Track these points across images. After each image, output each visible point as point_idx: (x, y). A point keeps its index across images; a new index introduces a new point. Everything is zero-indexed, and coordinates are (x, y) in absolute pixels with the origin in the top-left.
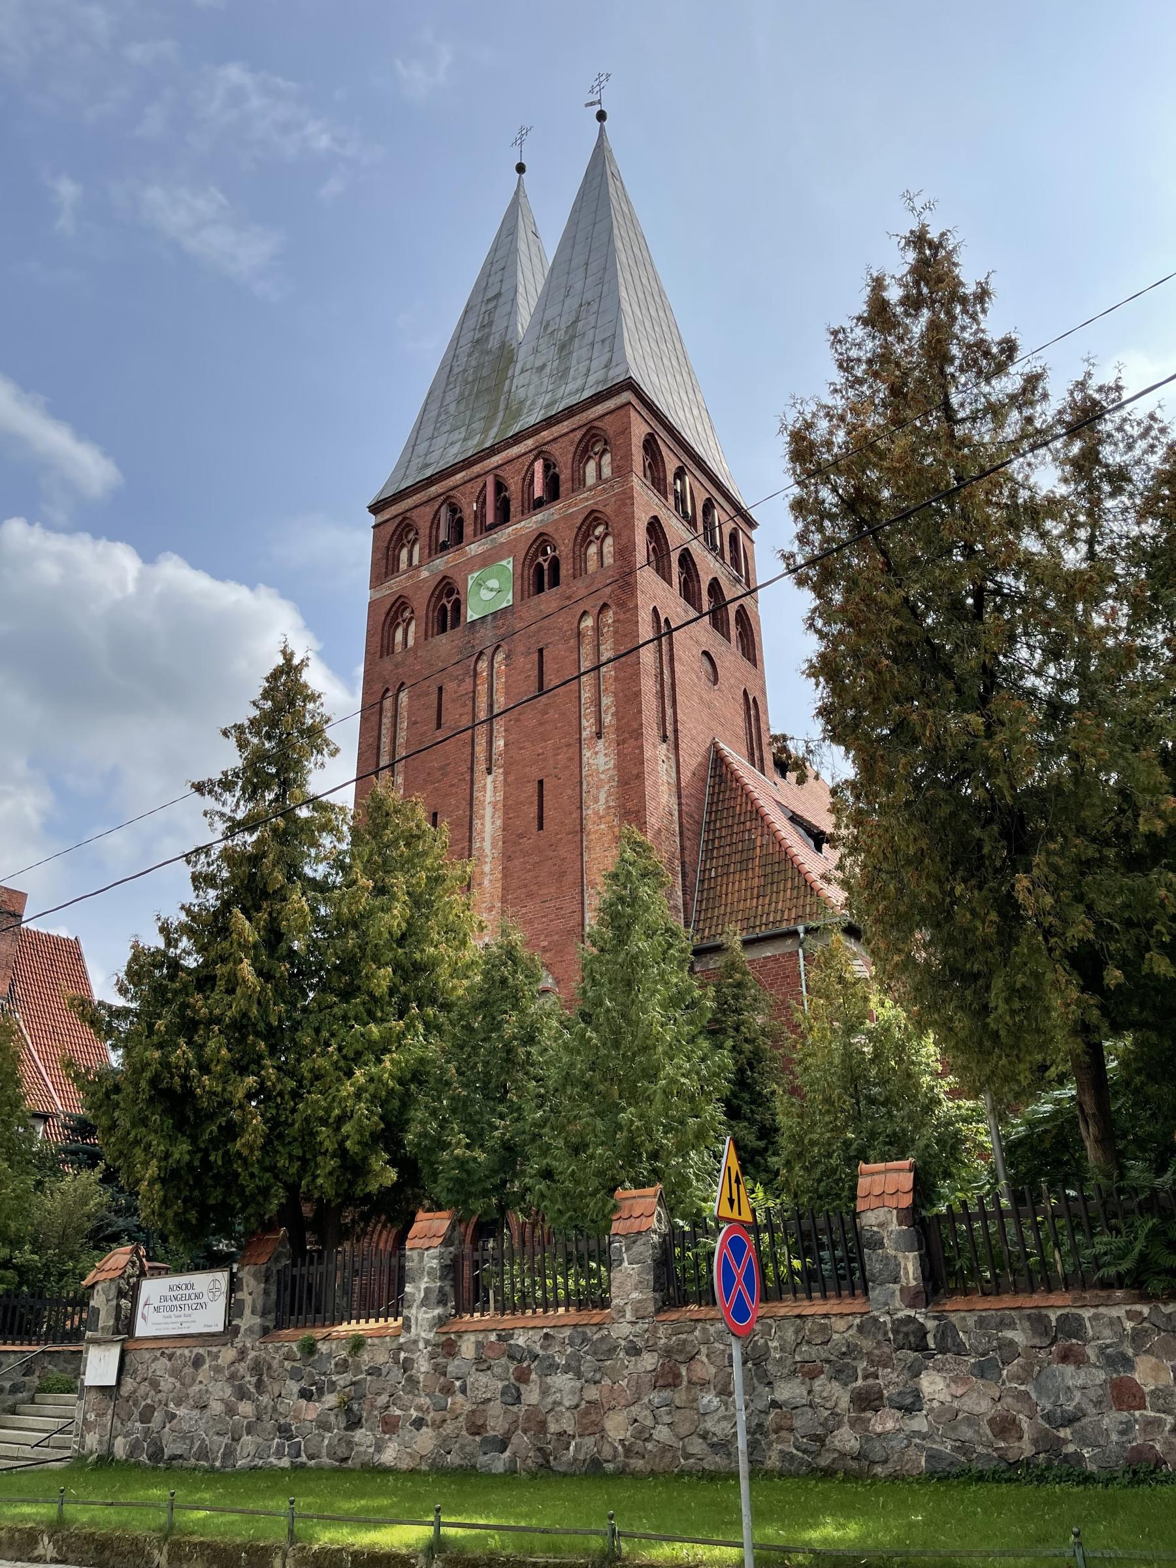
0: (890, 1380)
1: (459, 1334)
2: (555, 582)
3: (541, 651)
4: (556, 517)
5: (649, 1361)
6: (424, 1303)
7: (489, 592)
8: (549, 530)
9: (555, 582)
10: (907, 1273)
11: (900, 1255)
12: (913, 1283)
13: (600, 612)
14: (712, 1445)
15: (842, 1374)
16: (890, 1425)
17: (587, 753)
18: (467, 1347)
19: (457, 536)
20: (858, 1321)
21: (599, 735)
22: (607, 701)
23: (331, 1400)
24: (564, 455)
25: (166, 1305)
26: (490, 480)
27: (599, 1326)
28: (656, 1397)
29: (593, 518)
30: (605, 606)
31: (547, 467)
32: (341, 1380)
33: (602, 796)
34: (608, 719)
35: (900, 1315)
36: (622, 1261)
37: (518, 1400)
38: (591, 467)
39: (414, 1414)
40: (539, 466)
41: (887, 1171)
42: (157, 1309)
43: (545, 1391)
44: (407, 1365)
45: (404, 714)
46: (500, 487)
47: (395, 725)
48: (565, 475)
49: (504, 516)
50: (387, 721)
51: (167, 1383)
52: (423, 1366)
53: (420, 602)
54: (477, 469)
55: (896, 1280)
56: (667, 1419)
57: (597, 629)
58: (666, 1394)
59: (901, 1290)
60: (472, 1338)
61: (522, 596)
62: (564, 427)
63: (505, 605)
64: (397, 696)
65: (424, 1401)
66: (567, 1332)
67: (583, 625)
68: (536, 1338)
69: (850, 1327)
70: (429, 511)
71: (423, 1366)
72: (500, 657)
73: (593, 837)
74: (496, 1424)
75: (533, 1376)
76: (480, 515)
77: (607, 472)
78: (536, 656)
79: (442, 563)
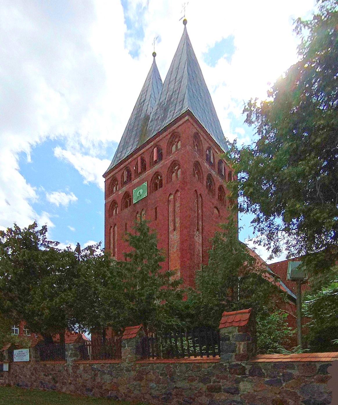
0: (225, 384)
1: (79, 364)
2: (161, 186)
3: (156, 208)
4: (161, 166)
5: (133, 374)
6: (70, 356)
7: (140, 193)
8: (160, 171)
9: (161, 186)
10: (240, 349)
11: (237, 343)
12: (242, 352)
13: (176, 193)
14: (153, 397)
15: (204, 380)
16: (223, 397)
17: (171, 236)
18: (81, 367)
19: (129, 178)
20: (214, 365)
21: (174, 230)
22: (177, 220)
23: (51, 377)
24: (164, 145)
25: (19, 355)
26: (139, 158)
27: (118, 364)
28: (135, 383)
29: (174, 163)
30: (177, 191)
31: (158, 151)
32: (53, 373)
33: (175, 247)
34: (177, 225)
35: (234, 363)
36: (125, 346)
37: (94, 380)
38: (174, 148)
39: (69, 381)
40: (155, 150)
41: (236, 314)
42: (17, 356)
43: (102, 379)
44: (67, 370)
45: (116, 232)
46: (143, 160)
47: (114, 236)
48: (164, 152)
49: (144, 169)
50: (112, 235)
51: (18, 371)
52: (71, 371)
53: (119, 202)
54: (135, 156)
55: (233, 351)
56: (139, 389)
57: (174, 198)
58: (138, 382)
59: (236, 355)
60: (83, 365)
61: (150, 193)
62: (165, 134)
63: (145, 196)
64: (114, 228)
65: (71, 379)
66: (108, 365)
67: (170, 198)
68: (100, 366)
69: (210, 367)
70: (121, 173)
71: (71, 371)
72: (143, 213)
73: (172, 258)
74: (89, 384)
75: (99, 375)
76: (136, 171)
77: (179, 147)
78: (154, 210)
79: (124, 189)
